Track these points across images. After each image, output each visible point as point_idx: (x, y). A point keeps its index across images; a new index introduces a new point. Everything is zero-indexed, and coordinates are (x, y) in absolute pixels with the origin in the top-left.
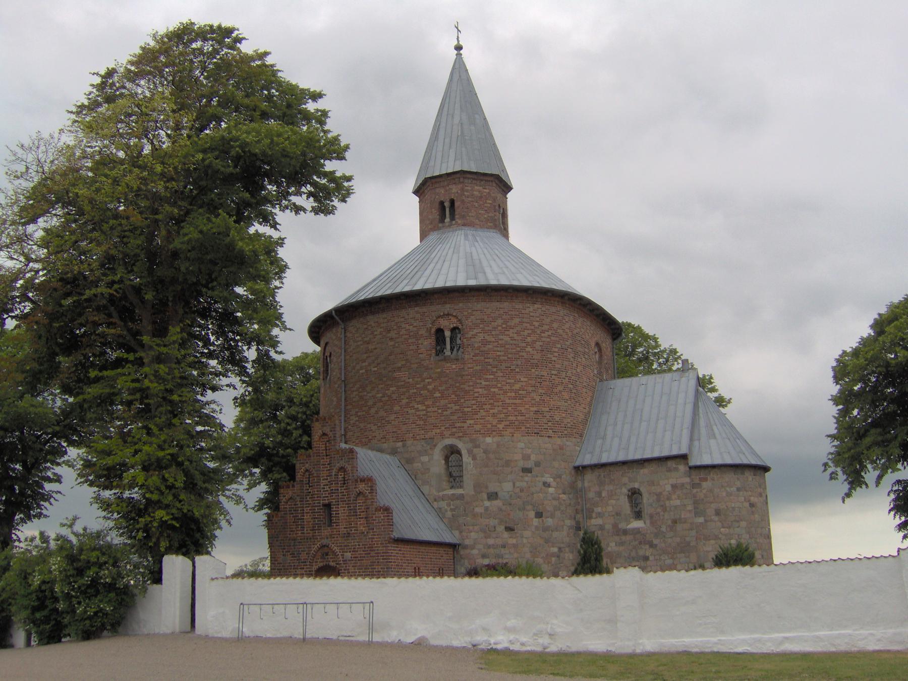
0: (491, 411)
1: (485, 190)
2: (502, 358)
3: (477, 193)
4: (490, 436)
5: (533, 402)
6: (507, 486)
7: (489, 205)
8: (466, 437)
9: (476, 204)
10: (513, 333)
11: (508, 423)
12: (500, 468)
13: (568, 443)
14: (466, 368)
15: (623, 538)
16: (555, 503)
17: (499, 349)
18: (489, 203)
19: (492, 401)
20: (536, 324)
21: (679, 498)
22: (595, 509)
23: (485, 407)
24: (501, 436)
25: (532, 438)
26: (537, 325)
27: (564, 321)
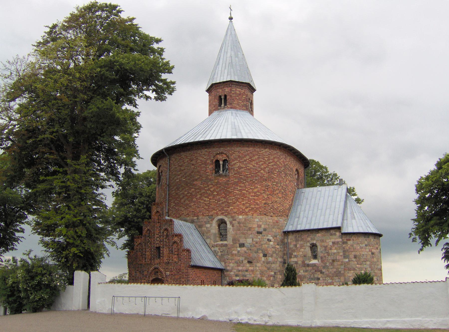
0: (242, 202)
2: (248, 176)
5: (264, 198)
6: (249, 241)
9: (238, 98)
11: (250, 209)
16: (273, 250)
17: (247, 171)
19: (243, 197)
20: (266, 159)
21: (336, 249)
23: (239, 200)
26: (266, 160)
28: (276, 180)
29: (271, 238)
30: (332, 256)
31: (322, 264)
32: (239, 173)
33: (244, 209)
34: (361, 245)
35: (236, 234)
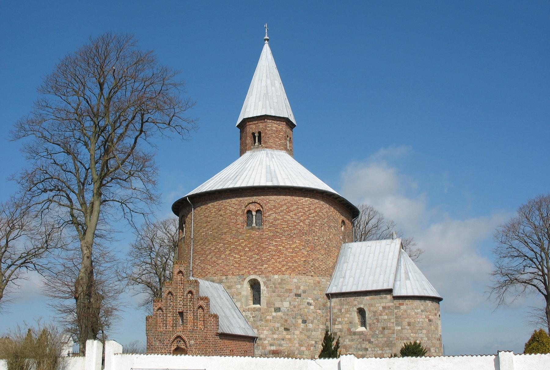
1: (279, 127)
2: (285, 229)
3: (275, 128)
4: (277, 274)
5: (303, 255)
6: (286, 304)
9: (274, 135)
11: (288, 267)
12: (282, 293)
13: (323, 280)
16: (315, 315)
17: (284, 223)
18: (282, 135)
19: (279, 254)
20: (307, 209)
21: (386, 314)
22: (337, 319)
23: (274, 257)
24: (283, 275)
27: (323, 208)
28: (318, 234)
30: (382, 323)
31: (371, 332)
32: (276, 226)
33: (280, 267)
34: (416, 310)
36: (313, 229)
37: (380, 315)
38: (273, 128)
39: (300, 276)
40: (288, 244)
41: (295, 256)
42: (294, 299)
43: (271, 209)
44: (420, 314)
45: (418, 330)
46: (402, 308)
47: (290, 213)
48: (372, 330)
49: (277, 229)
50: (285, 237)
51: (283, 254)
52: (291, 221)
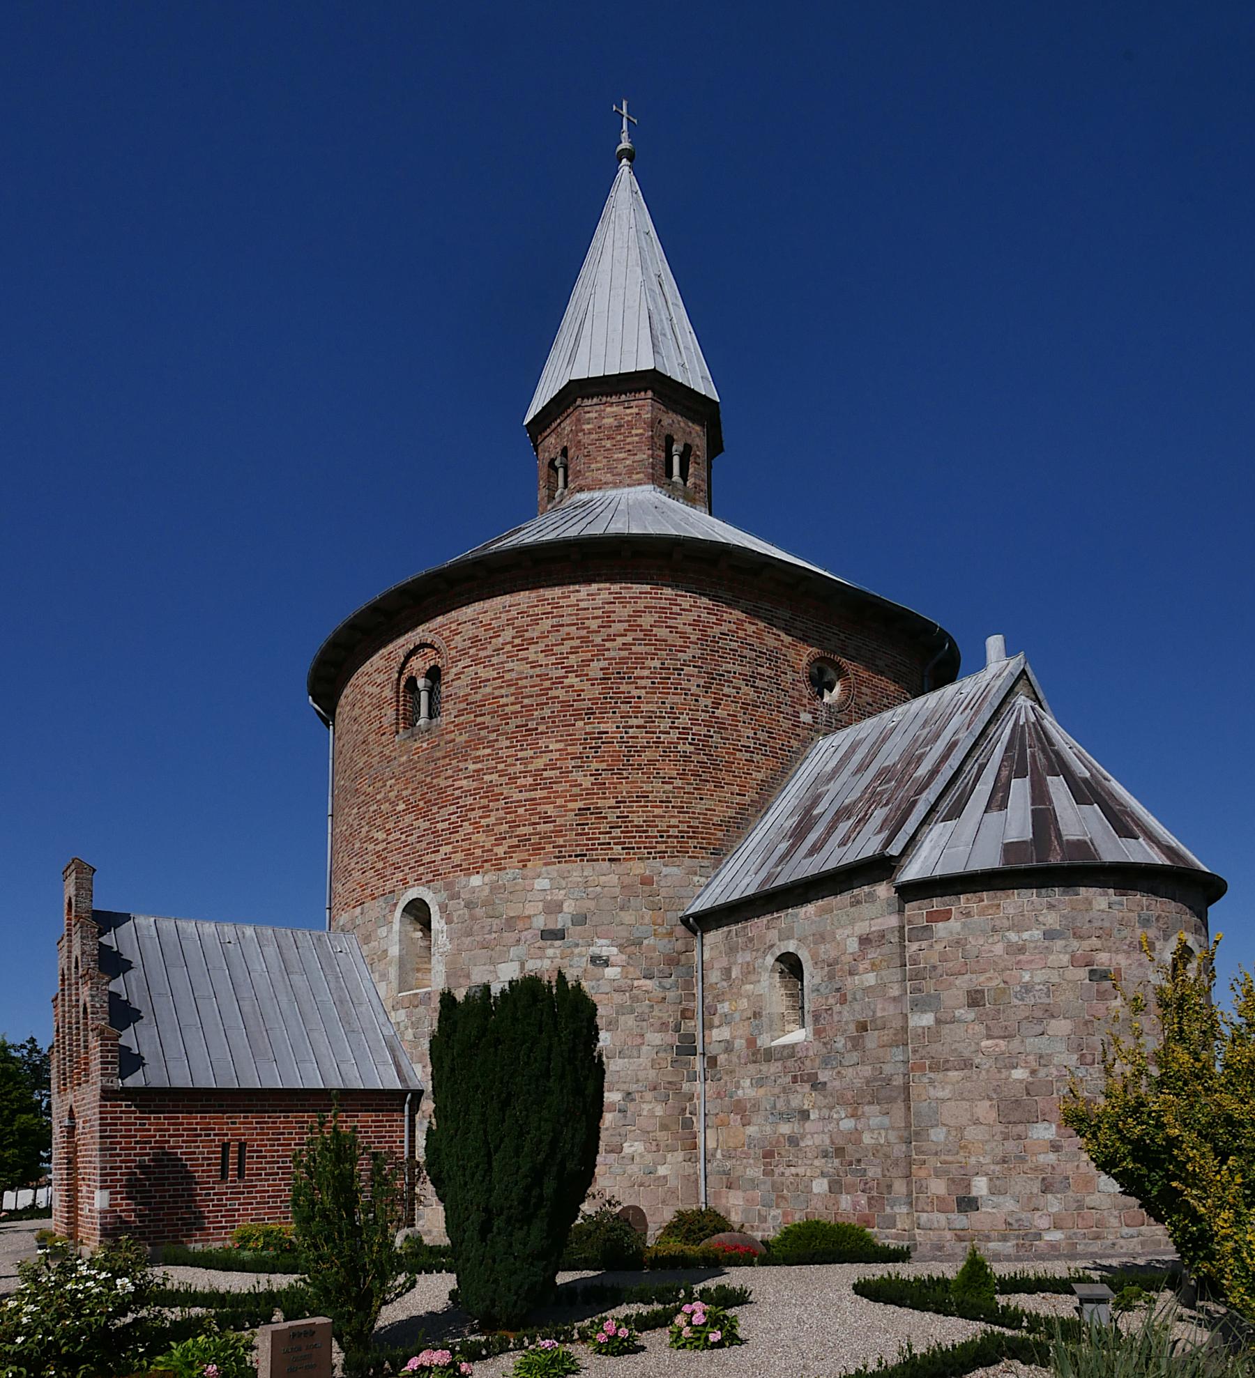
0: (484, 822)
1: (628, 411)
2: (508, 709)
3: (612, 420)
4: (478, 873)
5: (576, 790)
7: (636, 439)
8: (438, 880)
9: (608, 444)
10: (698, 686)
11: (515, 841)
12: (494, 935)
13: (665, 870)
14: (442, 743)
15: (764, 1067)
17: (503, 691)
18: (637, 435)
19: (484, 802)
20: (594, 624)
21: (874, 967)
22: (719, 1006)
23: (471, 815)
24: (499, 870)
25: (568, 866)
27: (676, 609)
28: (644, 707)
29: (604, 948)
30: (857, 1007)
31: (817, 1046)
33: (488, 846)
34: (1013, 936)
35: (459, 951)
36: (624, 693)
37: (851, 973)
38: (605, 421)
39: (563, 865)
40: (517, 760)
41: (544, 798)
42: (537, 951)
43: (464, 652)
44: (1035, 948)
45: (1025, 1024)
46: (942, 934)
47: (527, 649)
48: (823, 1035)
49: (481, 715)
50: (507, 739)
51: (498, 800)
52: (532, 677)
